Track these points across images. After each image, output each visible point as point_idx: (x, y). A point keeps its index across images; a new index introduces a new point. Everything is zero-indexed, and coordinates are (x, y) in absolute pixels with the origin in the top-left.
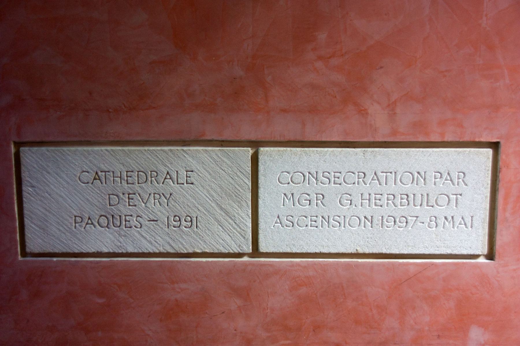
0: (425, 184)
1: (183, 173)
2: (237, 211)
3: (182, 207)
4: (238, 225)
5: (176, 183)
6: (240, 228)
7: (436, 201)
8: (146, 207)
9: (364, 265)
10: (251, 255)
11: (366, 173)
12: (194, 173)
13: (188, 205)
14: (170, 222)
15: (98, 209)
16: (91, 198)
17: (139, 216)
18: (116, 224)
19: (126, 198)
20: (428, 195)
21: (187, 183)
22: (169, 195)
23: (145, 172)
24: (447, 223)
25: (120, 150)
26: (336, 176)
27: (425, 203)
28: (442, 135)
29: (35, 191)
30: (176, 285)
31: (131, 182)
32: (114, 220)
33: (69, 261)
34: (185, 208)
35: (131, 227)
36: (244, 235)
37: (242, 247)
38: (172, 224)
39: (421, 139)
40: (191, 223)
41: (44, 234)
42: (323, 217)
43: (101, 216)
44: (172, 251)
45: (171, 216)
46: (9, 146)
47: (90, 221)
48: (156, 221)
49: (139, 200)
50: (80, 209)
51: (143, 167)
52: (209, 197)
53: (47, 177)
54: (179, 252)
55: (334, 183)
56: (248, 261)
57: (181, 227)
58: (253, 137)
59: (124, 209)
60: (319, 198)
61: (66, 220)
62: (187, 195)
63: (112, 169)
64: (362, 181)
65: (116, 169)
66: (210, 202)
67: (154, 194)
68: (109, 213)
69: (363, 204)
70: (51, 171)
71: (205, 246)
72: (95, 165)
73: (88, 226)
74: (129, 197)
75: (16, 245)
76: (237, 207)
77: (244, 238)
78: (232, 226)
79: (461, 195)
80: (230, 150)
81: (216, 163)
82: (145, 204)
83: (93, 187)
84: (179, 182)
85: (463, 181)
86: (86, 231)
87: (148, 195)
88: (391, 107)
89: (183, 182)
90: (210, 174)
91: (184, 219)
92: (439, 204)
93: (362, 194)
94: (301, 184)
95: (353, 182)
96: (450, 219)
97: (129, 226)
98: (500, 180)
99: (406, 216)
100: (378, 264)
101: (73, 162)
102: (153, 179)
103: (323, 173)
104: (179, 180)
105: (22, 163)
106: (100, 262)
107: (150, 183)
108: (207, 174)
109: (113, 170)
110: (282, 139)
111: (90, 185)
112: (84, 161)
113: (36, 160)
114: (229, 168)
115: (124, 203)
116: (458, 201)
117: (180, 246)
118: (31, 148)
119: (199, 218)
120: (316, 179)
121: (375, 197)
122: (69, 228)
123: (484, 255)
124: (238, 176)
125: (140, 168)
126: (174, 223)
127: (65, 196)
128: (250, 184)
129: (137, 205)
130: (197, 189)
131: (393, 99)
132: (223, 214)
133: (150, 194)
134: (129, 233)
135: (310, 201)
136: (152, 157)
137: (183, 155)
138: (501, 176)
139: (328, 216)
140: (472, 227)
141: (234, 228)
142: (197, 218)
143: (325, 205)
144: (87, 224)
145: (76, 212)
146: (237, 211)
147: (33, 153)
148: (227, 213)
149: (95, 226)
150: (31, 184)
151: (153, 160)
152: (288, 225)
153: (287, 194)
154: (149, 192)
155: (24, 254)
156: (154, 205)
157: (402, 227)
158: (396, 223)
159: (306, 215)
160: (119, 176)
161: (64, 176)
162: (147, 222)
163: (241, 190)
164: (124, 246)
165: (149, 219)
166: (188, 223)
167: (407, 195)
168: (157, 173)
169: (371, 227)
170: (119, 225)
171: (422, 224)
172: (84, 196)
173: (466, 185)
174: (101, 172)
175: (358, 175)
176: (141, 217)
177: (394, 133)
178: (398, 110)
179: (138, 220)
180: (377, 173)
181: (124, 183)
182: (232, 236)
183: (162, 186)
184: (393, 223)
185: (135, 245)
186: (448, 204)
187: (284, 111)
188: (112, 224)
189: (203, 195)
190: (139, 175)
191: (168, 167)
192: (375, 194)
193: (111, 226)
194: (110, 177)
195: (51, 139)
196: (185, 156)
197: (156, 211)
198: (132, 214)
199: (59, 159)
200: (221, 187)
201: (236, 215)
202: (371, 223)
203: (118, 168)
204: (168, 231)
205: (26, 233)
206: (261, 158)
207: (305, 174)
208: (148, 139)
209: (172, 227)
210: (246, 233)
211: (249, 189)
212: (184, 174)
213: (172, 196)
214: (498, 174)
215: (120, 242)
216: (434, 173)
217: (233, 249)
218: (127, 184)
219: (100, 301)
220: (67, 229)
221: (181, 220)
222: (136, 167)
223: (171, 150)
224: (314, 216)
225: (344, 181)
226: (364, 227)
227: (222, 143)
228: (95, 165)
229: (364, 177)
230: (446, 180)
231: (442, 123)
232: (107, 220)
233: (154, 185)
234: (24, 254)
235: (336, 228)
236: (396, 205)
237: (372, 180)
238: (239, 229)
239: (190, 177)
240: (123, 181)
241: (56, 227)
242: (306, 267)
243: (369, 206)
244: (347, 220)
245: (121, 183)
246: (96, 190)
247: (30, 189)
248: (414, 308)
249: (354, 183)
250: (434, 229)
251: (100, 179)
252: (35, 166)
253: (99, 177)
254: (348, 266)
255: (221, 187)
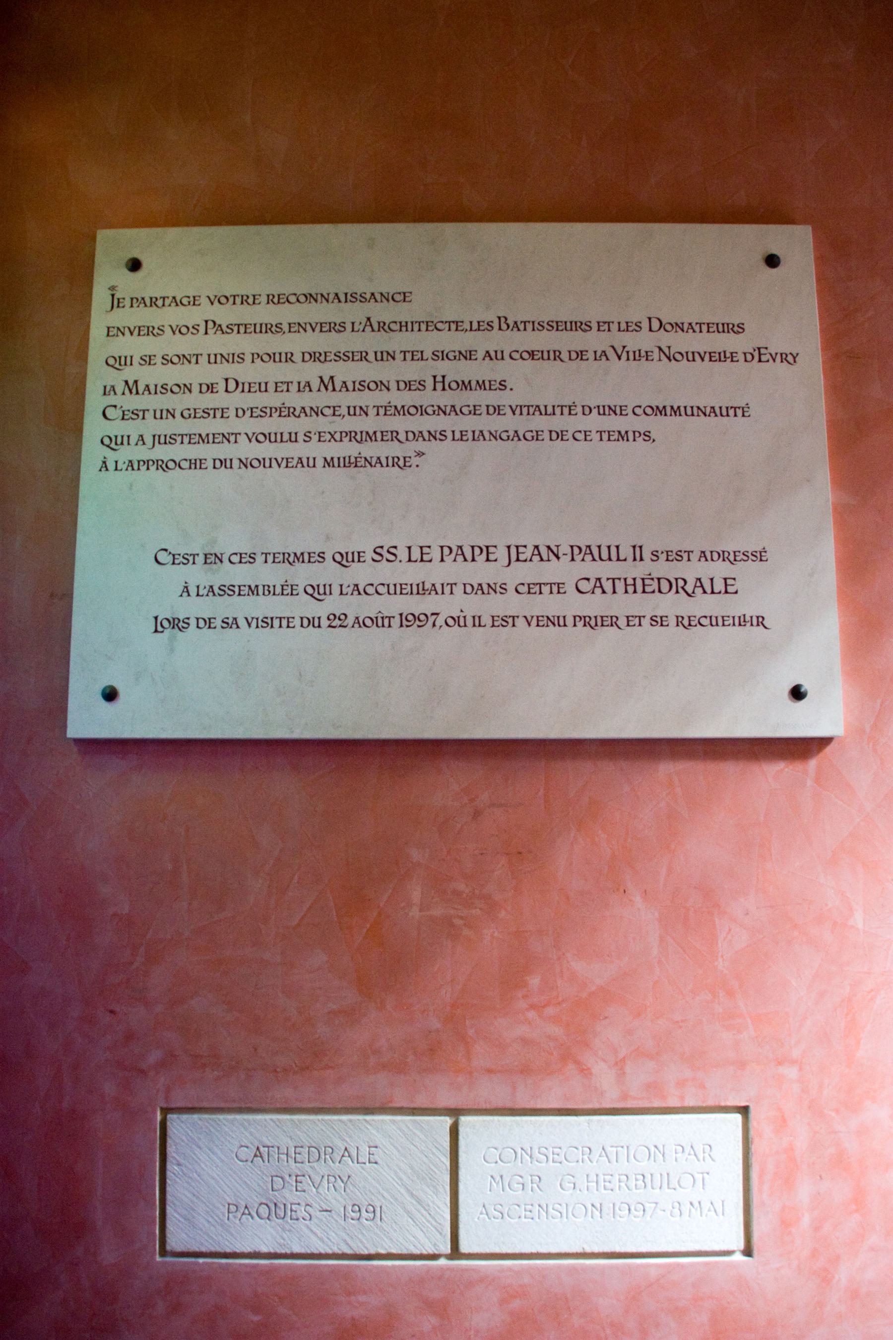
0: (664, 1161)
1: (365, 1150)
2: (432, 1199)
3: (363, 1193)
4: (433, 1218)
5: (356, 1162)
6: (436, 1221)
7: (679, 1182)
8: (318, 1192)
9: (593, 1268)
10: (450, 1257)
11: (592, 1149)
12: (378, 1149)
13: (370, 1191)
14: (347, 1214)
15: (258, 1196)
16: (249, 1180)
17: (308, 1205)
18: (279, 1215)
19: (293, 1181)
20: (668, 1174)
21: (369, 1162)
22: (347, 1177)
23: (318, 1147)
24: (693, 1210)
25: (287, 1119)
26: (555, 1152)
27: (665, 1185)
28: (682, 1098)
29: (182, 1170)
30: (353, 1298)
31: (300, 1161)
32: (277, 1210)
33: (219, 1264)
34: (366, 1194)
35: (297, 1219)
36: (440, 1230)
37: (438, 1246)
38: (349, 1216)
39: (656, 1104)
40: (373, 1214)
41: (190, 1226)
42: (539, 1206)
43: (261, 1204)
44: (349, 1251)
45: (348, 1205)
46: (155, 1113)
47: (246, 1211)
48: (330, 1211)
49: (309, 1184)
50: (235, 1195)
51: (315, 1142)
52: (397, 1180)
53: (197, 1153)
54: (358, 1253)
55: (553, 1161)
56: (446, 1265)
57: (361, 1220)
58: (452, 1103)
59: (289, 1195)
60: (534, 1181)
61: (218, 1208)
62: (369, 1177)
63: (277, 1144)
64: (587, 1159)
65: (281, 1143)
66: (399, 1187)
67: (328, 1176)
68: (271, 1200)
69: (590, 1188)
70: (202, 1145)
71: (391, 1245)
72: (255, 1138)
73: (244, 1216)
74: (296, 1179)
75: (155, 1241)
76: (432, 1194)
77: (441, 1234)
78: (426, 1218)
79: (708, 1173)
80: (424, 1120)
81: (406, 1137)
82: (317, 1189)
83: (253, 1167)
84: (360, 1160)
85: (710, 1155)
86: (241, 1223)
87: (321, 1177)
88: (620, 1065)
89: (364, 1161)
90: (399, 1151)
91: (364, 1210)
92: (682, 1185)
93: (587, 1175)
94: (513, 1163)
95: (576, 1160)
96: (696, 1204)
97: (295, 1217)
98: (753, 1152)
99: (643, 1203)
100: (611, 1267)
101: (229, 1135)
102: (328, 1157)
103: (539, 1149)
104: (360, 1158)
105: (168, 1134)
106: (257, 1265)
107: (323, 1162)
108: (395, 1152)
109: (278, 1145)
110: (488, 1106)
111: (249, 1163)
112: (243, 1134)
113: (186, 1132)
114: (423, 1144)
115: (290, 1187)
116: (705, 1181)
117: (360, 1245)
118: (180, 1116)
119: (384, 1208)
120: (531, 1157)
121: (604, 1179)
122: (220, 1219)
123: (740, 1251)
124: (433, 1154)
125: (312, 1142)
126: (353, 1214)
127: (217, 1177)
128: (448, 1164)
129: (306, 1190)
130: (381, 1170)
131: (621, 1056)
132: (415, 1202)
133: (323, 1177)
134: (295, 1226)
135: (523, 1185)
136: (327, 1129)
137: (364, 1125)
138: (753, 1148)
139: (547, 1205)
140: (723, 1214)
141: (428, 1221)
142: (381, 1207)
143: (542, 1189)
144: (243, 1214)
145: (231, 1198)
146: (432, 1199)
147: (182, 1122)
148: (419, 1201)
149: (252, 1218)
150: (178, 1161)
151: (328, 1132)
152: (496, 1216)
153: (494, 1175)
154: (322, 1174)
155: (163, 1252)
156: (328, 1191)
157: (638, 1217)
158: (631, 1212)
159: (519, 1203)
160: (286, 1152)
161: (219, 1152)
162: (318, 1213)
163: (437, 1172)
164: (288, 1244)
165: (321, 1209)
166: (369, 1214)
167: (643, 1176)
168: (332, 1149)
169: (601, 1217)
170: (283, 1216)
171: (663, 1212)
172: (241, 1178)
173: (713, 1160)
174: (264, 1147)
175: (583, 1151)
176: (311, 1206)
177: (625, 1097)
178: (628, 1069)
179: (306, 1210)
180: (605, 1148)
181: (291, 1161)
182: (426, 1232)
183: (339, 1166)
184: (627, 1212)
185: (302, 1243)
186: (693, 1186)
187: (490, 1071)
188: (274, 1216)
189: (389, 1178)
190: (310, 1152)
191: (347, 1141)
192: (604, 1175)
193: (272, 1217)
194: (274, 1154)
195: (205, 1104)
196: (367, 1128)
197: (330, 1198)
198: (300, 1202)
199: (212, 1130)
200: (412, 1168)
201: (431, 1205)
202: (601, 1213)
203: (285, 1142)
204: (344, 1225)
205: (168, 1225)
206: (462, 1130)
207: (516, 1150)
208: (321, 1106)
209: (350, 1220)
210: (444, 1227)
211: (447, 1169)
212: (366, 1151)
213: (350, 1179)
214: (750, 1146)
215: (284, 1239)
216: (674, 1147)
217: (427, 1248)
218: (295, 1162)
219: (256, 1318)
220: (218, 1220)
221: (361, 1210)
222: (308, 1141)
223: (351, 1121)
224: (528, 1205)
225: (566, 1159)
226: (592, 1217)
227: (415, 1111)
228: (255, 1138)
229: (590, 1154)
230: (689, 1154)
231: (681, 1084)
232: (268, 1209)
233: (328, 1164)
234: (163, 1252)
235: (556, 1220)
236: (630, 1188)
237: (600, 1156)
238: (433, 1222)
239: (373, 1154)
240: (290, 1159)
241: (204, 1218)
242: (518, 1273)
243: (597, 1190)
244: (570, 1209)
245: (287, 1162)
246: (256, 1170)
247: (176, 1168)
248: (657, 1326)
249: (578, 1161)
250: (678, 1218)
251: (261, 1157)
252: (184, 1138)
253: (260, 1153)
254: (573, 1270)
255: (412, 1168)
